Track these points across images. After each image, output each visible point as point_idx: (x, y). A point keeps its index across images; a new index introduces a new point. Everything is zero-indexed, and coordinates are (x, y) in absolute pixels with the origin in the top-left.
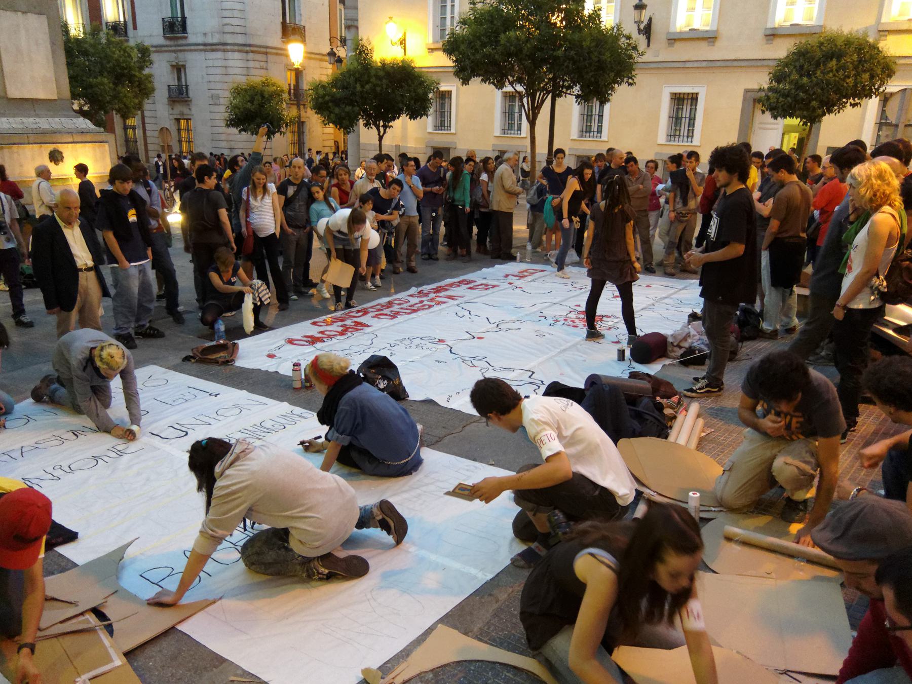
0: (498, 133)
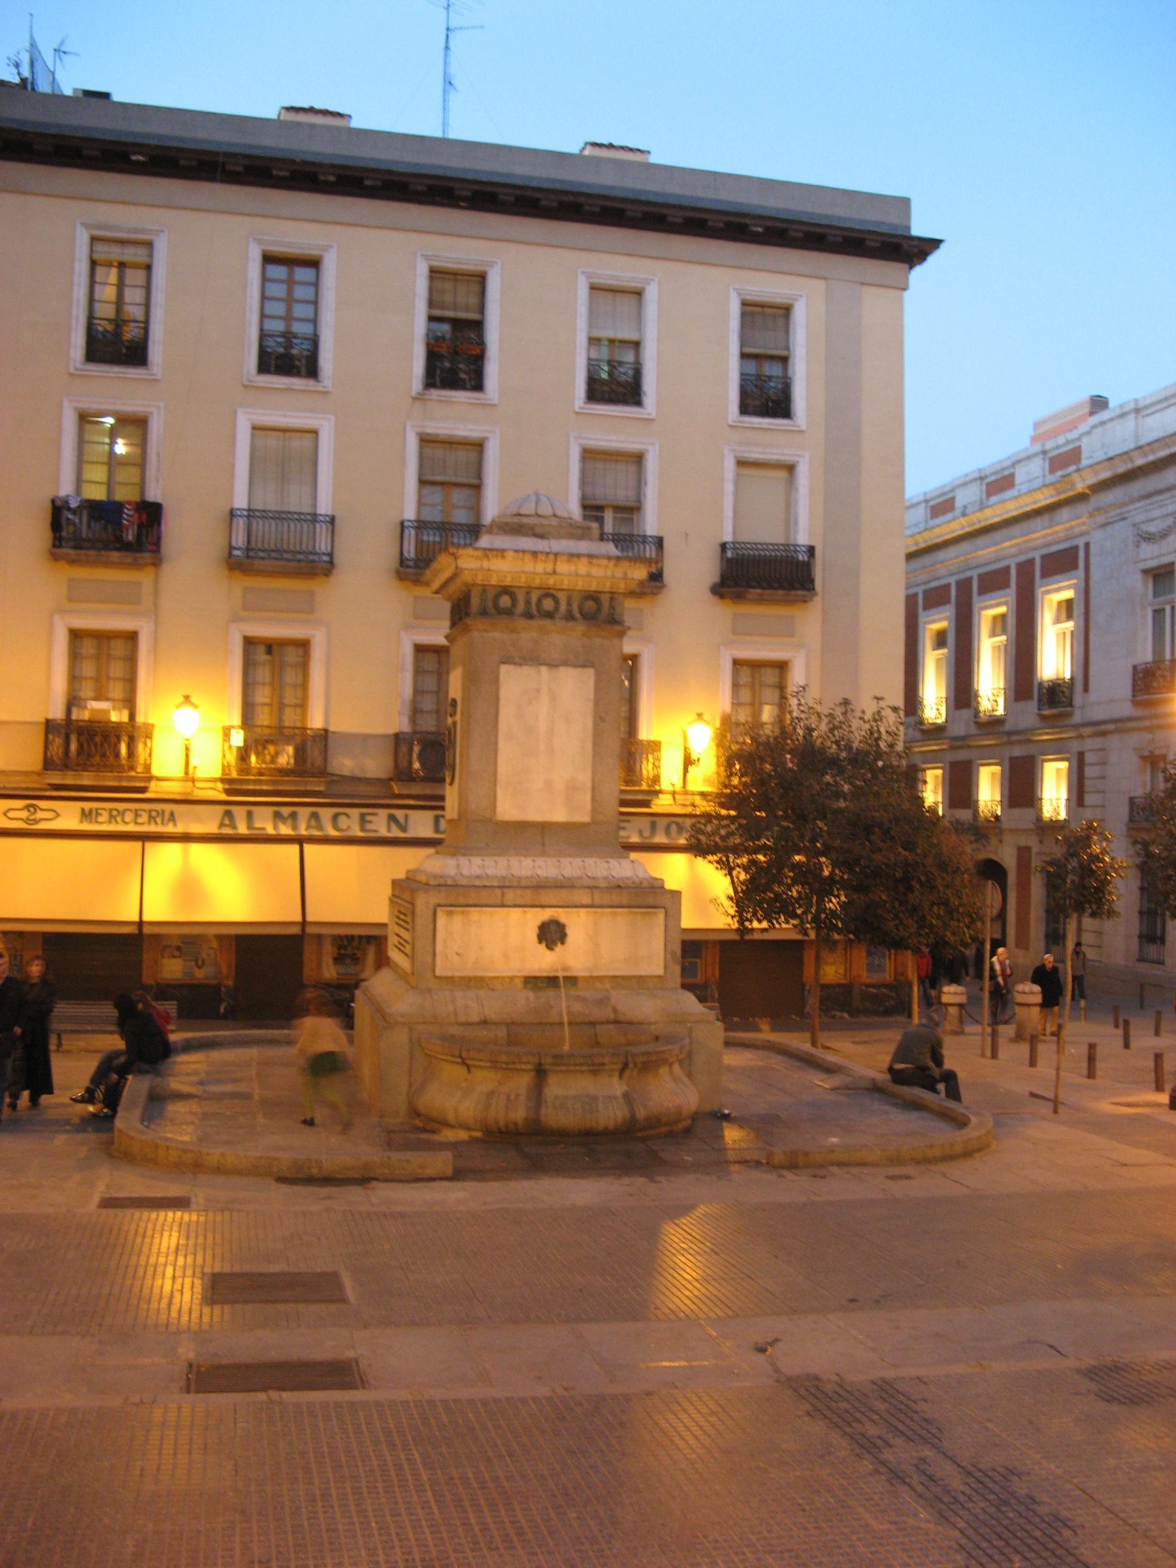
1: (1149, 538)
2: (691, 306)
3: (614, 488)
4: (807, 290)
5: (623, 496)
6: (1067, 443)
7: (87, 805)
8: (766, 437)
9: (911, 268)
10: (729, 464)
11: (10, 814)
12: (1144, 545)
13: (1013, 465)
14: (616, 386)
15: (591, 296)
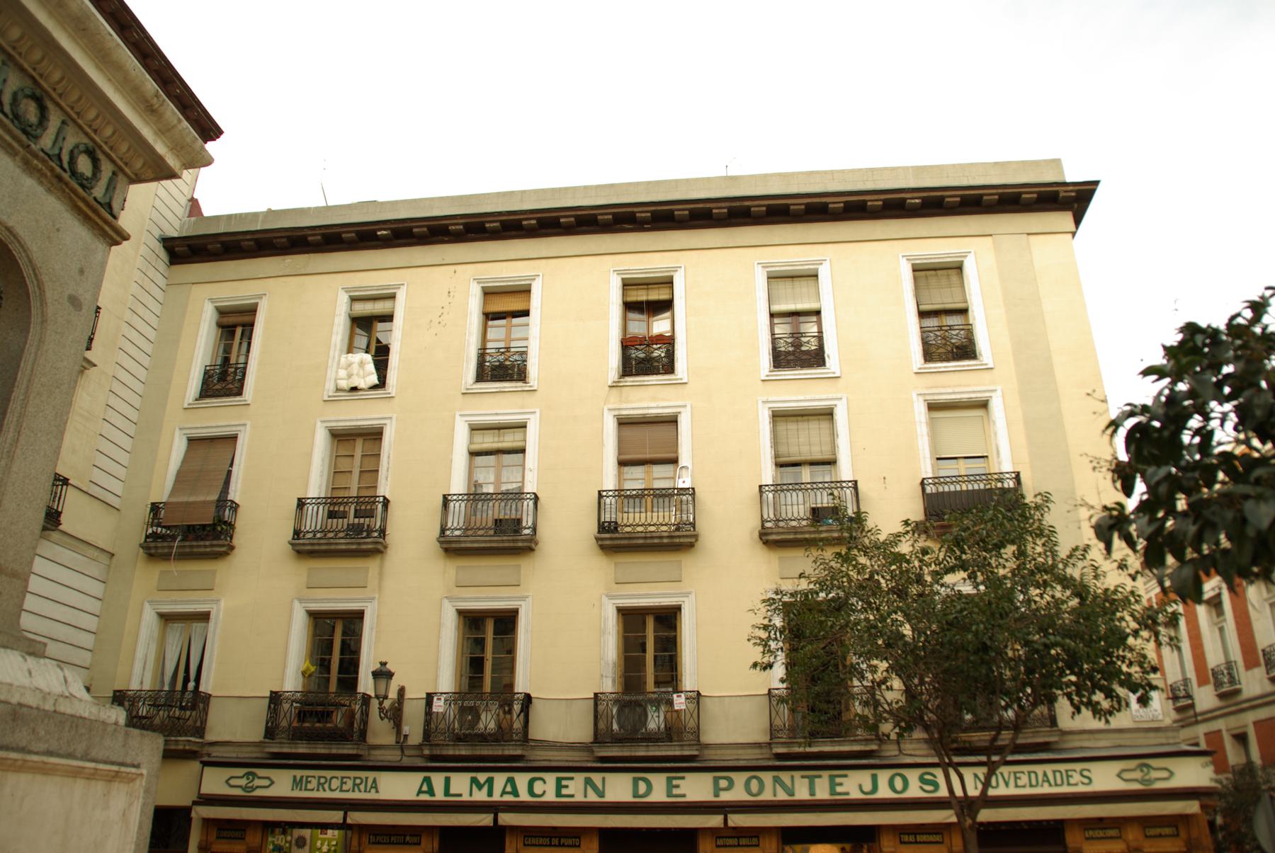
2: (866, 281)
3: (806, 441)
4: (985, 255)
7: (299, 773)
8: (955, 380)
10: (921, 408)
11: (232, 782)
14: (797, 352)
15: (932, 423)
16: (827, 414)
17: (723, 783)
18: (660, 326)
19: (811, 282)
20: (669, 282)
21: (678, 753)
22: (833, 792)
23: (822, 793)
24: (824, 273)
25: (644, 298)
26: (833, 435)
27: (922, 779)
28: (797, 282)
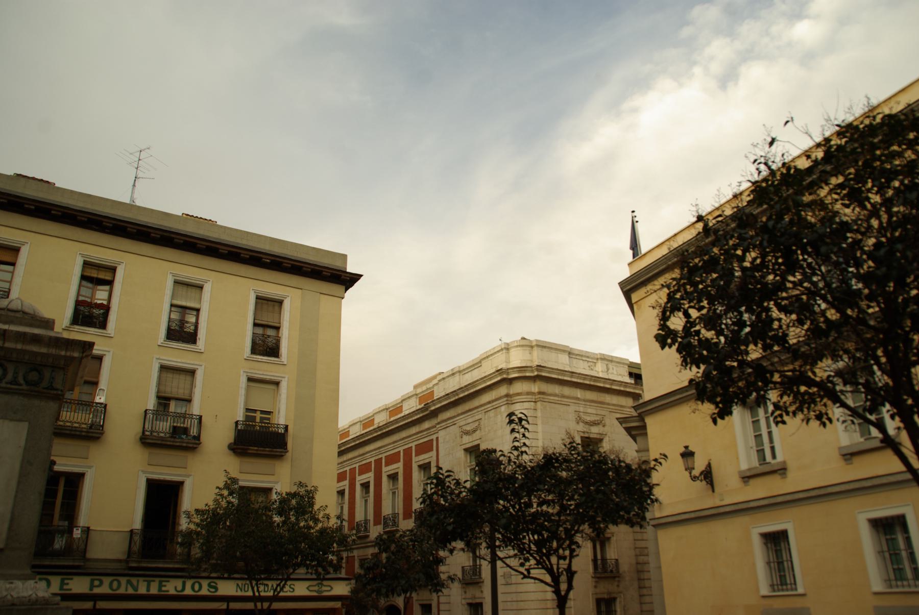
0: (765, 590)
1: (467, 433)
2: (228, 299)
3: (176, 386)
4: (294, 296)
5: (182, 393)
6: (427, 389)
8: (265, 367)
9: (346, 290)
10: (243, 380)
12: (464, 437)
13: (402, 401)
14: (182, 333)
15: (248, 388)
16: (192, 372)
17: (96, 583)
18: (101, 295)
19: (198, 290)
20: (113, 270)
21: (71, 564)
22: (160, 590)
23: (154, 590)
24: (207, 288)
25: (95, 276)
26: (192, 385)
27: (209, 585)
28: (190, 289)
